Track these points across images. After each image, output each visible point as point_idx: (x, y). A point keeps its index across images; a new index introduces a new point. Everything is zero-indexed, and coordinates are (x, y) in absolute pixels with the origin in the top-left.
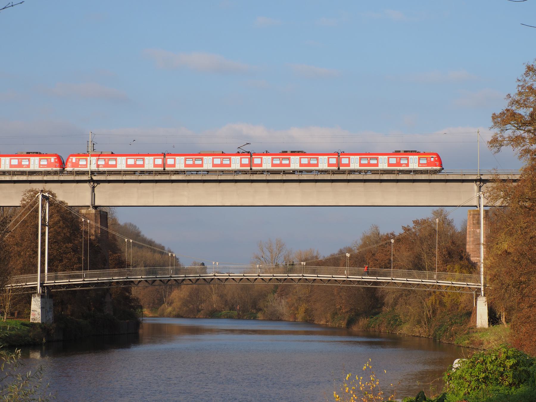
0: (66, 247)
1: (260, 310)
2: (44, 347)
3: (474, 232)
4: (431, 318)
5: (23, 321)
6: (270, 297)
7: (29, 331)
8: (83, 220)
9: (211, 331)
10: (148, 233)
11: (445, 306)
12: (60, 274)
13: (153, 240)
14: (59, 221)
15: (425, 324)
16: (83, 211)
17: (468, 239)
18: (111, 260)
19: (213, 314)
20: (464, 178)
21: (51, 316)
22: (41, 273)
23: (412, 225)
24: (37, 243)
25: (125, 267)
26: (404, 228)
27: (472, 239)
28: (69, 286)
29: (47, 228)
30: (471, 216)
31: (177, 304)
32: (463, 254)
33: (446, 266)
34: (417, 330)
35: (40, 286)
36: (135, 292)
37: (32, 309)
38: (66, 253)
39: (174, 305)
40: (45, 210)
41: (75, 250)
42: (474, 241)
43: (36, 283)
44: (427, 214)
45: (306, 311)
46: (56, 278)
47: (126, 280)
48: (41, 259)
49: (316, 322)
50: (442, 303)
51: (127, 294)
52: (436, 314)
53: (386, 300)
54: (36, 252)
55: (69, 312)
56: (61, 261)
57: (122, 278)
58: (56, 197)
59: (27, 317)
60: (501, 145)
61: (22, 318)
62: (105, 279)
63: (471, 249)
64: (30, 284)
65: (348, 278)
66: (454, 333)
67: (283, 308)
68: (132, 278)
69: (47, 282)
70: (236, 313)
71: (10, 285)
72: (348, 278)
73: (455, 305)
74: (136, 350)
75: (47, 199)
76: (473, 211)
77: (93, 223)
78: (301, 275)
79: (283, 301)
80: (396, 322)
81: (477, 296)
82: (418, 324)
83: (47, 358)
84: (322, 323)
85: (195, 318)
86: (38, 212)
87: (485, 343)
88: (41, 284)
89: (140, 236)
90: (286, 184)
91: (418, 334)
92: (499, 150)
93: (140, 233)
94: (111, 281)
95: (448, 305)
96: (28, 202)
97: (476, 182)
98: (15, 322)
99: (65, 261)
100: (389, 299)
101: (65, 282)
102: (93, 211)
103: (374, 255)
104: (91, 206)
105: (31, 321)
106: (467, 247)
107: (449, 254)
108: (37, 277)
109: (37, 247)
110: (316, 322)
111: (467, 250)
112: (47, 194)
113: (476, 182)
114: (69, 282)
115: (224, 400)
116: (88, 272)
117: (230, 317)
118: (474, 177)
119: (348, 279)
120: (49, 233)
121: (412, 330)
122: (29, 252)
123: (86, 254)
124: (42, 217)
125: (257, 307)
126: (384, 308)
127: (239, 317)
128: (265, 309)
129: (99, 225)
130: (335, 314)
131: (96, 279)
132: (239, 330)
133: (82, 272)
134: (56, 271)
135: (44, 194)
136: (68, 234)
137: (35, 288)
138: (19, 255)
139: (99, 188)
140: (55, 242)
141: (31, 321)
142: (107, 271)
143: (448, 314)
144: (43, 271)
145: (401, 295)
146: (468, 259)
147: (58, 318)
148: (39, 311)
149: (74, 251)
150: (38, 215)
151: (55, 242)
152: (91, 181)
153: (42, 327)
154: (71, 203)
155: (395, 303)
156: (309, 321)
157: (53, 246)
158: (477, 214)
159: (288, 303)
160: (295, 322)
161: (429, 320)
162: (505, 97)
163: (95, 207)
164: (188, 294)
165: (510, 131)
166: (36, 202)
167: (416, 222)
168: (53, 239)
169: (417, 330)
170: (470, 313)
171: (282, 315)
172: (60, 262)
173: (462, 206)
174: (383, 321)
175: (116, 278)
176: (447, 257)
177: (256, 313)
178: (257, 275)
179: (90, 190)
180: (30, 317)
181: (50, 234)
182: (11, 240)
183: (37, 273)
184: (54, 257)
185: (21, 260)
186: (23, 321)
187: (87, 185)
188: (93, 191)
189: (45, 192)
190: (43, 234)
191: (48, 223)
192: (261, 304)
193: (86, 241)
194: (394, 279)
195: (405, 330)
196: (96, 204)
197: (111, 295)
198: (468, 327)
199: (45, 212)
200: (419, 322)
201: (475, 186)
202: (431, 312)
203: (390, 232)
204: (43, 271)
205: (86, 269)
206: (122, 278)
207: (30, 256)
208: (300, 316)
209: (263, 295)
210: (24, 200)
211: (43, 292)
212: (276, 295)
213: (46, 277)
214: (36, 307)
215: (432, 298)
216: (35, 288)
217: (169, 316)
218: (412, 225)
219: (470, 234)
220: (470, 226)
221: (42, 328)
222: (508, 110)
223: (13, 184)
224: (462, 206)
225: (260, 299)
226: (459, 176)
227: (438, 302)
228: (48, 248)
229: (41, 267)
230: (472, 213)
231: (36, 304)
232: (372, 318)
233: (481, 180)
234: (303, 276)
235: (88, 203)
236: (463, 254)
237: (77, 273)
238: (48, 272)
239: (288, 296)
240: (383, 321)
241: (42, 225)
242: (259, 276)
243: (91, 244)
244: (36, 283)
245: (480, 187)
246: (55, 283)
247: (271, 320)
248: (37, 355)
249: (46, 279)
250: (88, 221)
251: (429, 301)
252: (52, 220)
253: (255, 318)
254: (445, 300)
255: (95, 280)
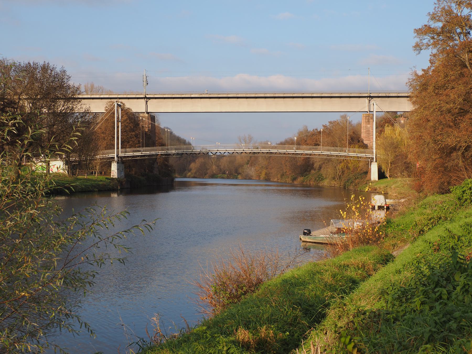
0: (131, 135)
1: (239, 174)
2: (119, 192)
3: (366, 126)
4: (341, 176)
5: (107, 177)
6: (245, 166)
7: (110, 182)
8: (141, 118)
9: (212, 184)
10: (177, 133)
11: (349, 169)
12: (128, 150)
13: (180, 136)
14: (127, 119)
15: (338, 179)
16: (141, 115)
17: (362, 131)
18: (157, 143)
19: (213, 176)
20: (360, 95)
21: (123, 174)
22: (117, 149)
23: (328, 124)
24: (114, 132)
25: (166, 146)
26: (324, 126)
27: (364, 131)
28: (133, 157)
29: (120, 123)
30: (364, 118)
31: (193, 171)
32: (360, 139)
33: (350, 146)
34: (333, 183)
35: (117, 157)
36: (172, 161)
37: (112, 170)
38: (131, 138)
39: (192, 171)
40: (119, 113)
41: (136, 136)
42: (366, 132)
43: (114, 155)
44: (336, 118)
45: (266, 174)
46: (126, 152)
47: (166, 153)
48: (117, 141)
49: (271, 180)
50: (348, 168)
51: (167, 163)
52: (344, 174)
53: (315, 165)
54: (114, 137)
55: (133, 173)
56: (128, 142)
57: (163, 152)
58: (125, 105)
59: (109, 175)
60: (421, 49)
61: (107, 175)
62: (153, 153)
63: (364, 137)
64: (111, 155)
65: (295, 152)
66: (357, 184)
67: (252, 172)
68: (170, 152)
69: (120, 155)
70: (226, 175)
71: (99, 156)
72: (295, 152)
73: (356, 168)
74: (173, 194)
75: (120, 106)
76: (366, 114)
77: (147, 120)
78: (268, 150)
79: (252, 168)
80: (321, 178)
81: (371, 162)
82: (333, 180)
83: (121, 196)
84: (275, 180)
85: (203, 178)
86: (114, 114)
87: (378, 189)
88: (117, 155)
89: (172, 134)
90: (257, 99)
91: (333, 185)
92: (419, 53)
93: (172, 132)
94: (157, 154)
95: (352, 168)
96: (109, 108)
97: (367, 98)
98: (102, 178)
99: (131, 142)
100: (316, 165)
101: (131, 154)
102: (147, 115)
103: (306, 141)
104: (146, 112)
105: (111, 177)
106: (362, 135)
107: (352, 139)
108: (115, 152)
109: (114, 134)
110: (271, 180)
111: (362, 137)
112: (120, 103)
113: (367, 98)
114: (133, 154)
115: (47, 293)
116: (144, 148)
117: (223, 178)
118: (366, 95)
119: (296, 152)
120: (121, 126)
121: (330, 183)
122: (110, 137)
123: (143, 139)
124: (117, 116)
125: (238, 172)
126: (313, 172)
127: (228, 178)
128: (242, 173)
129: (150, 122)
130: (282, 175)
131: (149, 152)
132: (228, 184)
133: (141, 149)
134: (125, 148)
135: (118, 103)
136: (132, 127)
137: (113, 158)
138: (104, 139)
139: (150, 102)
140: (125, 132)
141: (111, 177)
142: (155, 148)
143: (351, 174)
144: (118, 148)
145: (324, 163)
146: (363, 142)
147: (127, 176)
148: (116, 171)
149: (136, 137)
150: (115, 116)
151: (125, 132)
152: (145, 98)
153: (118, 180)
154: (134, 110)
155: (320, 168)
156: (267, 179)
157: (124, 134)
158: (367, 116)
159: (256, 170)
160: (259, 180)
161: (340, 177)
162: (427, 14)
163: (148, 113)
164: (199, 165)
165: (427, 39)
166: (113, 108)
167: (330, 123)
168: (124, 130)
169: (333, 183)
170: (367, 172)
171: (252, 176)
172: (128, 143)
173: (359, 112)
174: (312, 178)
175: (160, 152)
176: (350, 141)
177: (238, 175)
178: (242, 150)
179: (145, 103)
180: (111, 175)
181: (122, 127)
182: (99, 130)
183: (115, 149)
184: (125, 140)
185: (105, 142)
186: (107, 177)
187: (143, 100)
188: (147, 103)
189: (119, 102)
190: (118, 127)
191: (121, 120)
192: (240, 171)
193: (143, 132)
194: (322, 152)
195: (326, 183)
196: (148, 111)
197: (157, 163)
198: (366, 180)
199: (119, 114)
200: (334, 178)
201: (366, 100)
202: (341, 172)
203: (315, 128)
204: (118, 148)
205: (143, 147)
206: (163, 152)
207: (110, 139)
208: (263, 176)
209: (241, 166)
210: (107, 107)
211: (118, 160)
212: (248, 165)
213: (120, 151)
214: (114, 168)
215: (342, 164)
216: (113, 158)
217: (189, 177)
218: (328, 124)
219: (363, 128)
220: (364, 123)
221: (118, 181)
222: (426, 26)
223: (101, 100)
224: (359, 112)
225: (239, 168)
226: (358, 94)
227: (345, 166)
228: (121, 135)
229: (117, 146)
230: (365, 115)
231: (114, 167)
232: (305, 176)
233: (370, 97)
234: (269, 151)
235: (144, 111)
236: (360, 139)
237: (138, 149)
238: (121, 148)
239: (255, 166)
240: (312, 178)
241: (117, 121)
242: (244, 151)
243: (146, 134)
244: (114, 155)
245: (370, 100)
246: (125, 155)
247: (246, 179)
248: (115, 195)
249: (120, 153)
250: (144, 119)
251: (340, 167)
252: (123, 119)
253: (237, 178)
254: (350, 165)
255: (148, 153)
